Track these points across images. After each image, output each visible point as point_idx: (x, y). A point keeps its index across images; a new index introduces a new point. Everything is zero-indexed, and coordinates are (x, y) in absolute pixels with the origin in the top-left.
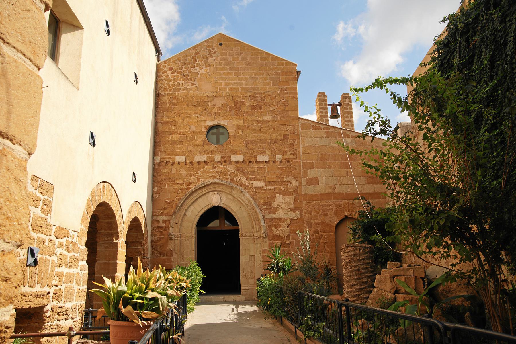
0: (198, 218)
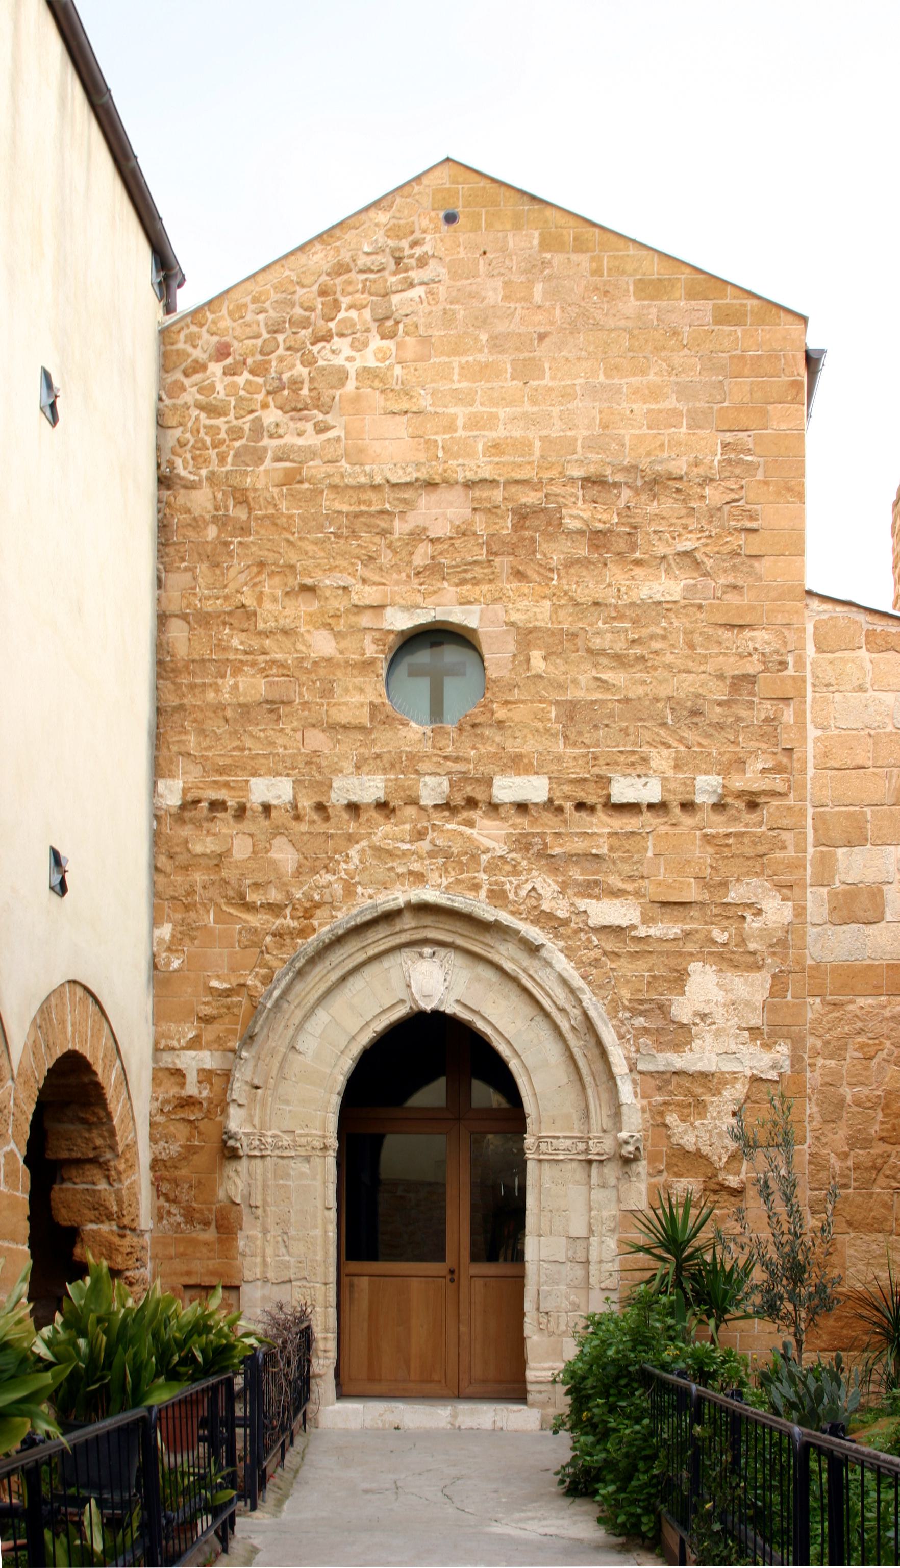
0: (347, 1064)
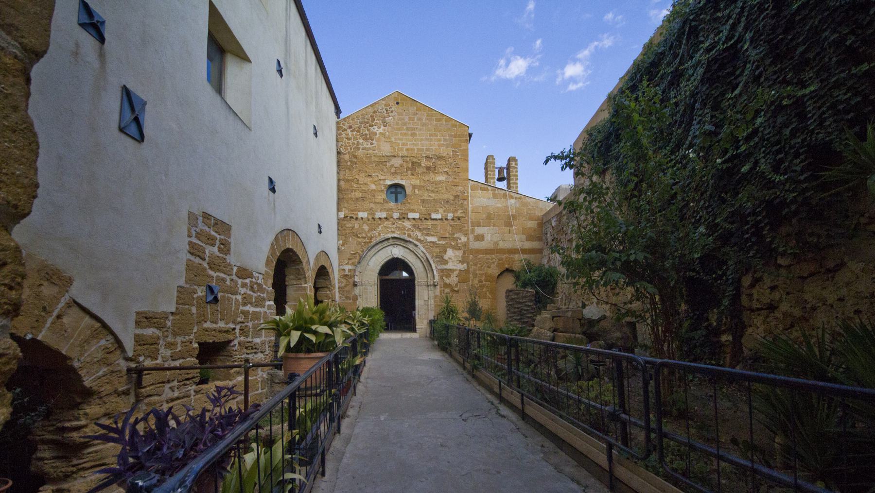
0: (379, 268)
